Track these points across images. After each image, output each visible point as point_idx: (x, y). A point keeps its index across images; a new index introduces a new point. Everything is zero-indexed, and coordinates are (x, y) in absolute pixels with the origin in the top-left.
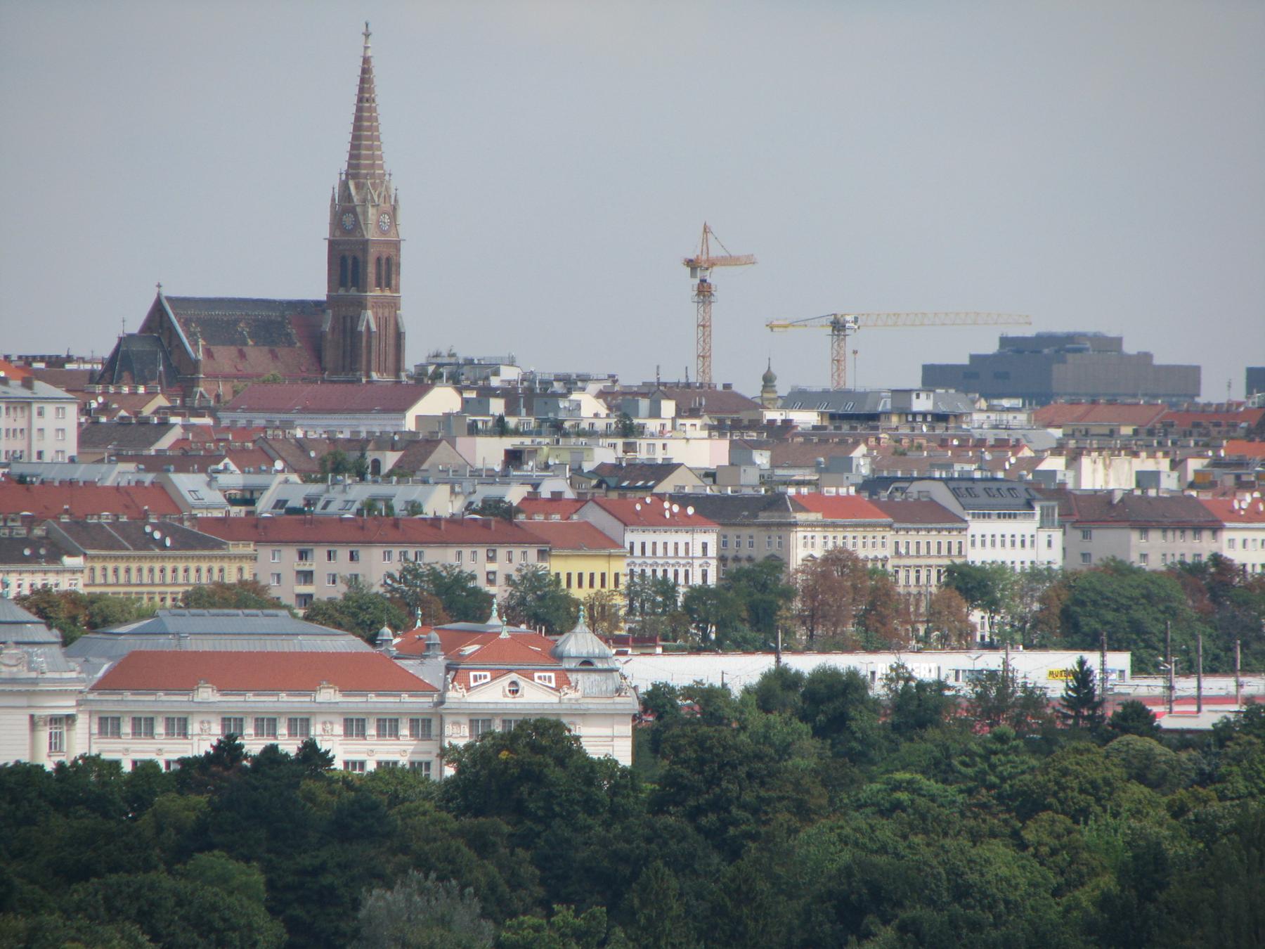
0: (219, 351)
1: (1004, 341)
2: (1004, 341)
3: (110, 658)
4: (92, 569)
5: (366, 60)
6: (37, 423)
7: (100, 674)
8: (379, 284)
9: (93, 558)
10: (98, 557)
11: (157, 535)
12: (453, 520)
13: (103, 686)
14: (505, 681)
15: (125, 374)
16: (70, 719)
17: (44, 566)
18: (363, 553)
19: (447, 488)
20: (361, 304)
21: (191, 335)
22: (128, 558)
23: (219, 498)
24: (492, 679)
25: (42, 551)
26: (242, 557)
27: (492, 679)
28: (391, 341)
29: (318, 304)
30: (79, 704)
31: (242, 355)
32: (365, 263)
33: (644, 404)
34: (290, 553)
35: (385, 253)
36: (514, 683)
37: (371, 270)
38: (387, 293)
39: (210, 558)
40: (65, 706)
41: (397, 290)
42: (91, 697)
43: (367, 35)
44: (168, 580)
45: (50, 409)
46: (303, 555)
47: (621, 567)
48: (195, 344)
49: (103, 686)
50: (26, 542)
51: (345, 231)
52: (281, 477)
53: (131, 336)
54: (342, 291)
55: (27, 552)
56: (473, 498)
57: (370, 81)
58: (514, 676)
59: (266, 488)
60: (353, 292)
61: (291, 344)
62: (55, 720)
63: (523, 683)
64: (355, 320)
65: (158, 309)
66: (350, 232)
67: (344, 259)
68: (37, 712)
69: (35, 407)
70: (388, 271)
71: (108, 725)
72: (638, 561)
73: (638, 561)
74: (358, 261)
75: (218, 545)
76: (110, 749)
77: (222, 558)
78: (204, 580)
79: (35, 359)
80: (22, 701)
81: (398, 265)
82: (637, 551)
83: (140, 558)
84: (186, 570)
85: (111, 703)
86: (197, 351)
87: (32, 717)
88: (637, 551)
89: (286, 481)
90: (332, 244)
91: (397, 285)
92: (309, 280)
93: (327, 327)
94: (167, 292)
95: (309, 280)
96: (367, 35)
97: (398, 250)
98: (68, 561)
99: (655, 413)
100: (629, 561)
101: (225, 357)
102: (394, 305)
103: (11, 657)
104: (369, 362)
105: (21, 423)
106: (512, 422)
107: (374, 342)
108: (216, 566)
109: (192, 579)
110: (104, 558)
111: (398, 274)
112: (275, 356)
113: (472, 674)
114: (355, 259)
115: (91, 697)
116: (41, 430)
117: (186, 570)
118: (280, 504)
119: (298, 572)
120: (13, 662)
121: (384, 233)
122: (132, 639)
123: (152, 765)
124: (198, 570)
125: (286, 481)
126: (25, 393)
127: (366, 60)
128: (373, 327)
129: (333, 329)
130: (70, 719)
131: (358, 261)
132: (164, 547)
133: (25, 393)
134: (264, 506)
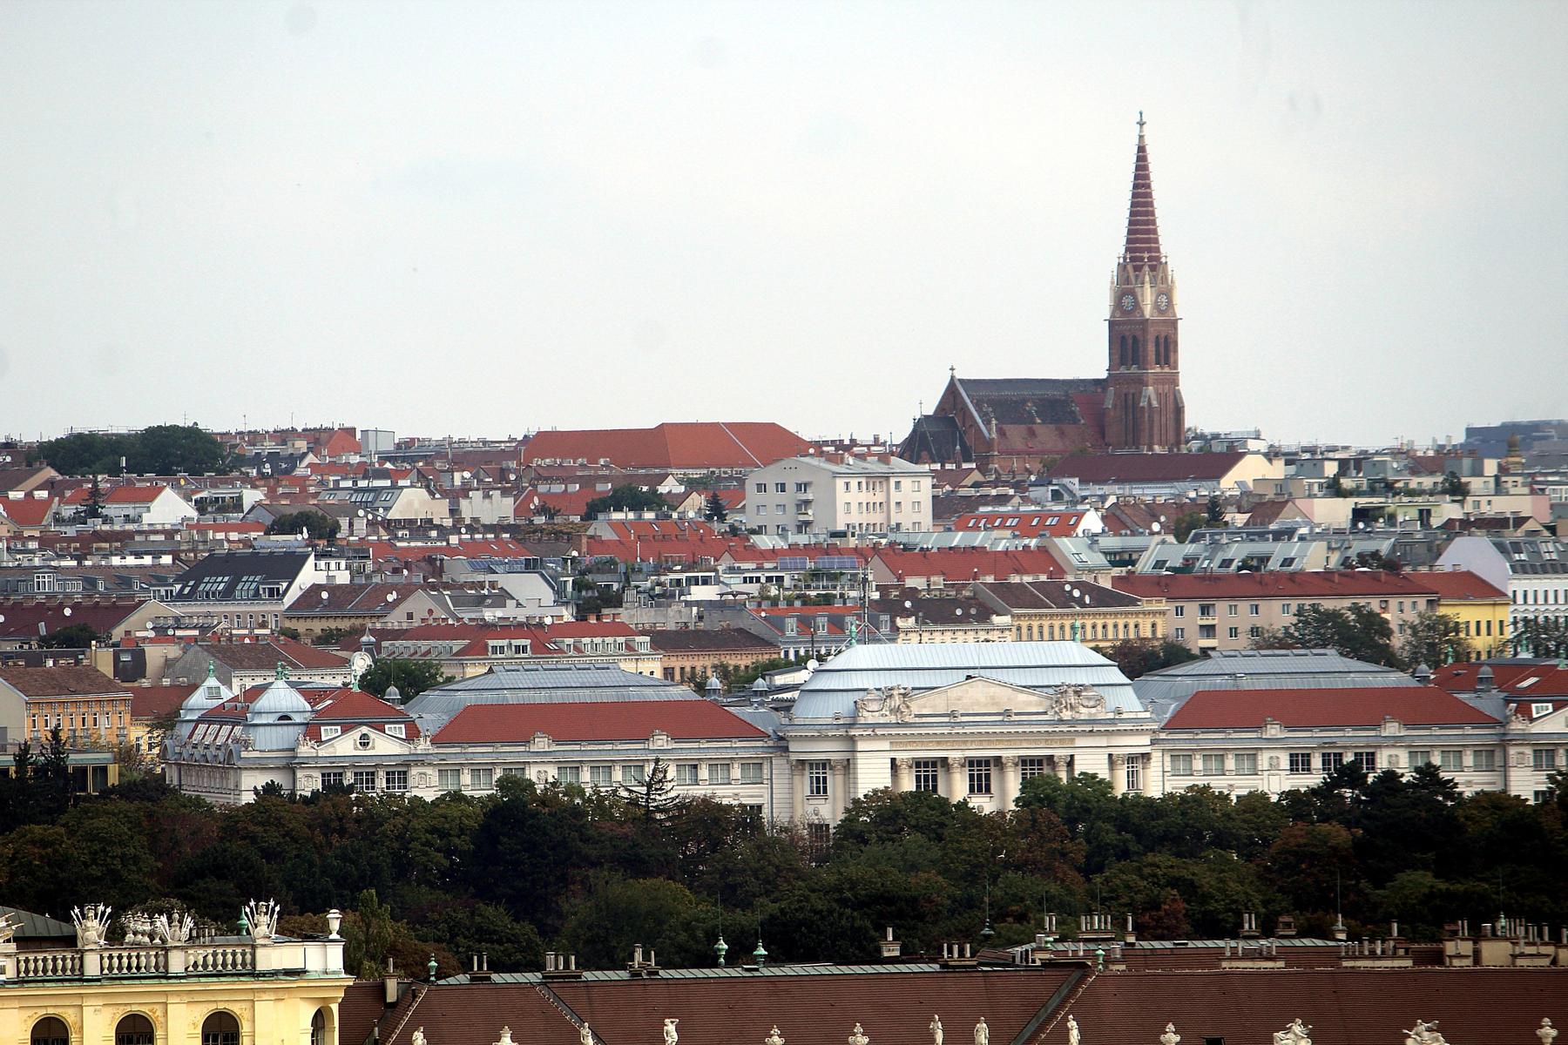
0: (1010, 429)
1: (1471, 432)
2: (1471, 432)
3: (1175, 699)
4: (1019, 628)
5: (1141, 149)
6: (895, 496)
7: (1168, 715)
8: (1158, 363)
9: (1019, 616)
10: (1024, 615)
11: (1076, 593)
12: (1327, 575)
13: (1170, 726)
14: (356, 734)
15: (924, 454)
16: (1146, 757)
17: (976, 626)
18: (1264, 605)
19: (1324, 544)
20: (1141, 382)
21: (984, 415)
22: (1052, 615)
23: (1101, 560)
24: (1555, 710)
25: (973, 611)
26: (1154, 613)
27: (1555, 710)
28: (1171, 416)
29: (1097, 382)
30: (1153, 742)
31: (1032, 433)
32: (1145, 341)
33: (1467, 463)
34: (1192, 608)
35: (1164, 331)
36: (364, 736)
37: (1151, 348)
38: (1167, 370)
39: (1127, 614)
40: (1140, 743)
41: (1176, 367)
42: (1163, 736)
43: (1141, 124)
44: (1100, 636)
45: (906, 483)
46: (1205, 610)
47: (1506, 614)
48: (987, 423)
49: (1170, 726)
50: (956, 602)
51: (1125, 313)
52: (1157, 538)
53: (927, 417)
54: (1123, 370)
55: (959, 612)
56: (1349, 553)
57: (1146, 168)
58: (365, 729)
59: (1146, 549)
60: (1134, 369)
61: (1075, 421)
62: (1132, 759)
63: (373, 735)
64: (1137, 396)
65: (952, 390)
66: (1130, 312)
67: (1123, 338)
68: (1114, 751)
69: (893, 481)
70: (1167, 349)
71: (1181, 757)
72: (1522, 608)
73: (1522, 608)
74: (1141, 341)
75: (1133, 602)
76: (1218, 784)
77: (1137, 613)
78: (1132, 636)
79: (826, 443)
80: (1103, 741)
81: (1176, 343)
82: (1520, 600)
83: (1062, 615)
84: (1094, 627)
85: (1182, 740)
86: (989, 431)
87: (1110, 755)
88: (1520, 600)
89: (1163, 542)
90: (1112, 324)
91: (1176, 362)
92: (1085, 357)
93: (1109, 404)
94: (958, 376)
95: (1085, 357)
96: (1141, 124)
97: (1176, 329)
98: (996, 619)
99: (1478, 472)
100: (1512, 608)
101: (1016, 433)
102: (1173, 380)
103: (1089, 699)
104: (1151, 436)
105: (880, 497)
106: (1346, 483)
107: (1156, 418)
108: (1132, 622)
109: (1121, 636)
110: (1030, 616)
111: (1176, 351)
112: (1062, 434)
113: (1534, 706)
114: (1135, 338)
115: (1163, 736)
116: (898, 504)
117: (1094, 627)
118: (1159, 564)
119: (1202, 626)
120: (1092, 703)
121: (1161, 312)
122: (1188, 681)
123: (1264, 797)
124: (1115, 626)
125: (1163, 542)
126: (883, 468)
127: (1141, 149)
128: (1155, 404)
129: (1115, 406)
130: (1146, 757)
131: (1141, 341)
132: (1083, 605)
133: (883, 468)
134: (1144, 566)
